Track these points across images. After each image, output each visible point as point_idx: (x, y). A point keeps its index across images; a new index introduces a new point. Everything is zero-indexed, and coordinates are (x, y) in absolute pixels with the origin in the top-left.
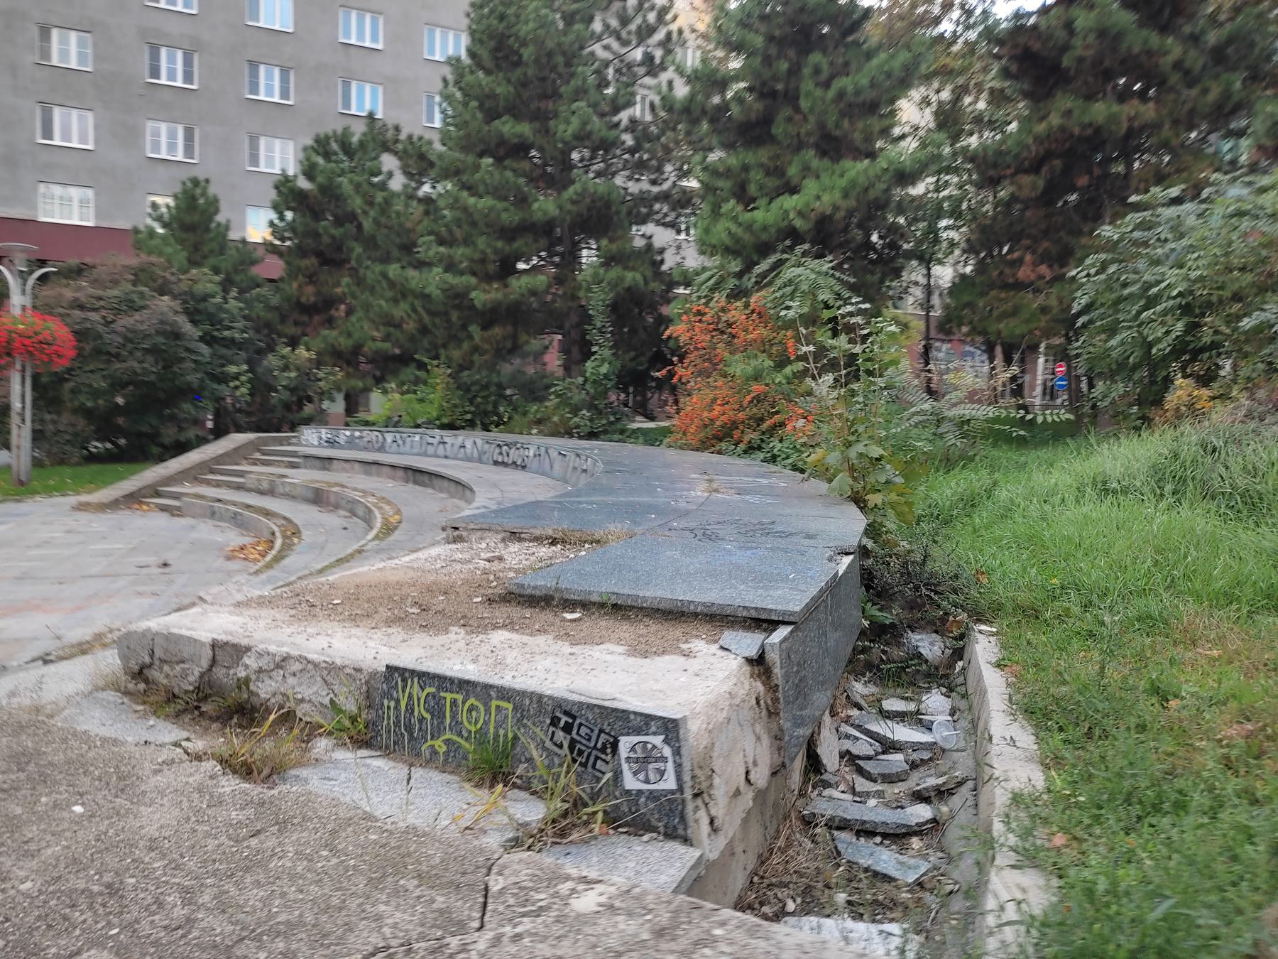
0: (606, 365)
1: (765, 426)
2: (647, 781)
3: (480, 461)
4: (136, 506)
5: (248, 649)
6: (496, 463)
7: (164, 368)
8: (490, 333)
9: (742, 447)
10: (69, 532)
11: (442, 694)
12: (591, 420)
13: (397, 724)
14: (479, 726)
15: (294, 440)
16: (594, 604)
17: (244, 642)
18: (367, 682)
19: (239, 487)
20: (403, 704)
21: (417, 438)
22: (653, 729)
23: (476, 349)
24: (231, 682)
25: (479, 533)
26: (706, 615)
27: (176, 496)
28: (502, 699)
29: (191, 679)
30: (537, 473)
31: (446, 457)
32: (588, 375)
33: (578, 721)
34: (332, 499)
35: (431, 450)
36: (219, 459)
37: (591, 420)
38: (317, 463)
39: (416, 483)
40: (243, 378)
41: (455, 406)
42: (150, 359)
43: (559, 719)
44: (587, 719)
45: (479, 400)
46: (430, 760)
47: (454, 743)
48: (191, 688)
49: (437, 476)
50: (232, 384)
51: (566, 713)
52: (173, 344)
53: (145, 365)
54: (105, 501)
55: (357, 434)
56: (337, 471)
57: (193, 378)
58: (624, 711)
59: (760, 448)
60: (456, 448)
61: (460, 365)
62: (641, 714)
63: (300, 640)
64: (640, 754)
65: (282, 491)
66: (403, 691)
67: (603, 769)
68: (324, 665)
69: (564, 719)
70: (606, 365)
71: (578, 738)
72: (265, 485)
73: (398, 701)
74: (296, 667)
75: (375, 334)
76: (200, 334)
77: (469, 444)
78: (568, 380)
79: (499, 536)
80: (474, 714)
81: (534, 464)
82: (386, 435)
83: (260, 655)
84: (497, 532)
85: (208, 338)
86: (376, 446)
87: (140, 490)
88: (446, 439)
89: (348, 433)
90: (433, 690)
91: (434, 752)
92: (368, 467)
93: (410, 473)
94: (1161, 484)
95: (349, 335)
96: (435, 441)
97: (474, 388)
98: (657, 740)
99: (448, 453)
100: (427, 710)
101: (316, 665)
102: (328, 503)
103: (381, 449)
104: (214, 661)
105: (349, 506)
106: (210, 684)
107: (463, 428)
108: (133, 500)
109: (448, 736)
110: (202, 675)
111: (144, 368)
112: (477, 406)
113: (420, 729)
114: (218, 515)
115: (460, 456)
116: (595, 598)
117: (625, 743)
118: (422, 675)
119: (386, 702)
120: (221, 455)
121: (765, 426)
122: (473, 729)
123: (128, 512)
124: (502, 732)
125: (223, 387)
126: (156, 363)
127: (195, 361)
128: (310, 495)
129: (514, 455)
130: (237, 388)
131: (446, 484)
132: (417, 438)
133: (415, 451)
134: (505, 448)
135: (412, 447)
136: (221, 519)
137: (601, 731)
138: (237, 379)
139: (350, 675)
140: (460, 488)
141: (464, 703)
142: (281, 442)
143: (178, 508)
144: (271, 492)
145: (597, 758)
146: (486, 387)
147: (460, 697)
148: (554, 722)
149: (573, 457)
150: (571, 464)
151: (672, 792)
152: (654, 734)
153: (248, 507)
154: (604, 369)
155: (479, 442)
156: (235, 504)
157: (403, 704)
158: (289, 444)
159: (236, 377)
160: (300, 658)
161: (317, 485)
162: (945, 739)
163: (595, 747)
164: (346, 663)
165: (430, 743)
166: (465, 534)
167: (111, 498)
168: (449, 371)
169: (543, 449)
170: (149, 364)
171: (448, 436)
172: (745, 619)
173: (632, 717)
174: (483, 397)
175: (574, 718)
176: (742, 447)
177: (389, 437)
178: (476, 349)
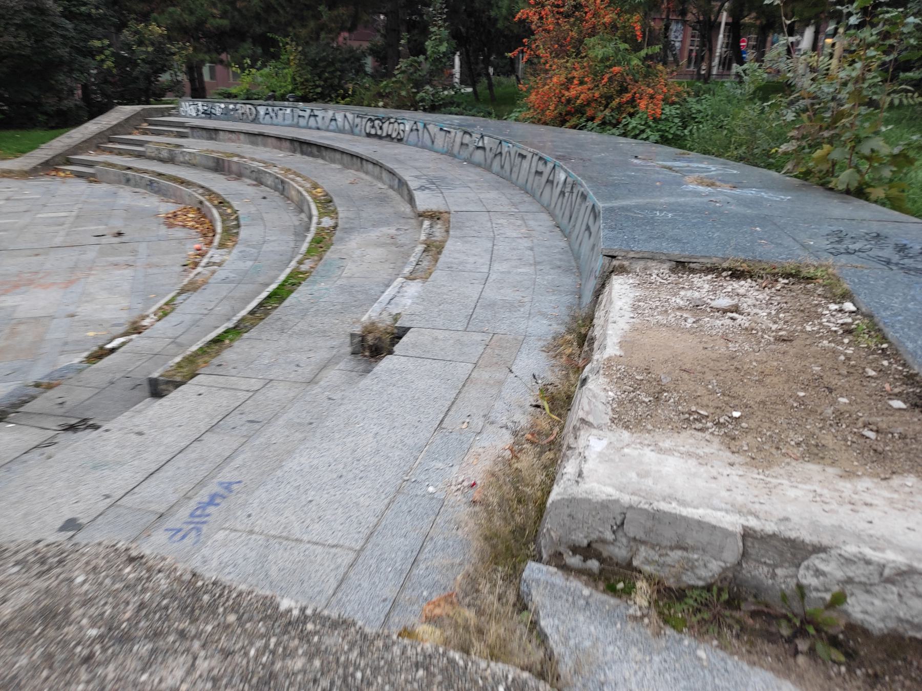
0: (445, 44)
1: (614, 104)
3: (352, 132)
4: (54, 173)
5: (819, 549)
6: (369, 135)
7: (36, 41)
8: (335, 13)
10: (8, 199)
15: (173, 112)
19: (140, 155)
21: (288, 111)
23: (322, 27)
25: (641, 264)
27: (90, 164)
29: (703, 573)
30: (416, 145)
31: (318, 129)
32: (428, 53)
34: (234, 168)
35: (302, 122)
36: (115, 129)
38: (204, 133)
39: (303, 153)
40: (107, 52)
41: (307, 80)
42: (23, 33)
49: (327, 148)
50: (98, 58)
52: (40, 19)
53: (19, 40)
54: (26, 168)
55: (231, 106)
56: (224, 141)
57: (64, 52)
60: (327, 120)
65: (182, 159)
70: (445, 44)
72: (165, 154)
75: (215, 11)
76: (61, 9)
77: (339, 117)
78: (412, 58)
79: (666, 266)
81: (413, 137)
82: (259, 108)
83: (848, 561)
84: (662, 262)
85: (67, 13)
86: (251, 118)
87: (54, 157)
88: (316, 113)
89: (223, 106)
92: (253, 138)
93: (297, 145)
95: (192, 12)
96: (307, 114)
97: (322, 64)
102: (230, 172)
103: (255, 120)
104: (745, 554)
105: (254, 175)
107: (315, 100)
108: (49, 167)
111: (19, 43)
112: (325, 80)
114: (132, 182)
115: (331, 128)
120: (116, 125)
121: (614, 104)
123: (47, 178)
125: (89, 60)
126: (29, 37)
127: (62, 36)
128: (211, 164)
130: (103, 61)
131: (338, 156)
132: (288, 111)
133: (287, 122)
134: (377, 122)
135: (284, 119)
136: (135, 186)
138: (102, 53)
142: (162, 112)
143: (93, 175)
144: (171, 160)
146: (332, 63)
149: (460, 134)
150: (458, 140)
153: (160, 175)
155: (350, 116)
156: (145, 172)
158: (170, 115)
159: (101, 51)
161: (215, 155)
166: (626, 263)
167: (31, 166)
169: (420, 126)
170: (22, 38)
174: (329, 73)
177: (262, 110)
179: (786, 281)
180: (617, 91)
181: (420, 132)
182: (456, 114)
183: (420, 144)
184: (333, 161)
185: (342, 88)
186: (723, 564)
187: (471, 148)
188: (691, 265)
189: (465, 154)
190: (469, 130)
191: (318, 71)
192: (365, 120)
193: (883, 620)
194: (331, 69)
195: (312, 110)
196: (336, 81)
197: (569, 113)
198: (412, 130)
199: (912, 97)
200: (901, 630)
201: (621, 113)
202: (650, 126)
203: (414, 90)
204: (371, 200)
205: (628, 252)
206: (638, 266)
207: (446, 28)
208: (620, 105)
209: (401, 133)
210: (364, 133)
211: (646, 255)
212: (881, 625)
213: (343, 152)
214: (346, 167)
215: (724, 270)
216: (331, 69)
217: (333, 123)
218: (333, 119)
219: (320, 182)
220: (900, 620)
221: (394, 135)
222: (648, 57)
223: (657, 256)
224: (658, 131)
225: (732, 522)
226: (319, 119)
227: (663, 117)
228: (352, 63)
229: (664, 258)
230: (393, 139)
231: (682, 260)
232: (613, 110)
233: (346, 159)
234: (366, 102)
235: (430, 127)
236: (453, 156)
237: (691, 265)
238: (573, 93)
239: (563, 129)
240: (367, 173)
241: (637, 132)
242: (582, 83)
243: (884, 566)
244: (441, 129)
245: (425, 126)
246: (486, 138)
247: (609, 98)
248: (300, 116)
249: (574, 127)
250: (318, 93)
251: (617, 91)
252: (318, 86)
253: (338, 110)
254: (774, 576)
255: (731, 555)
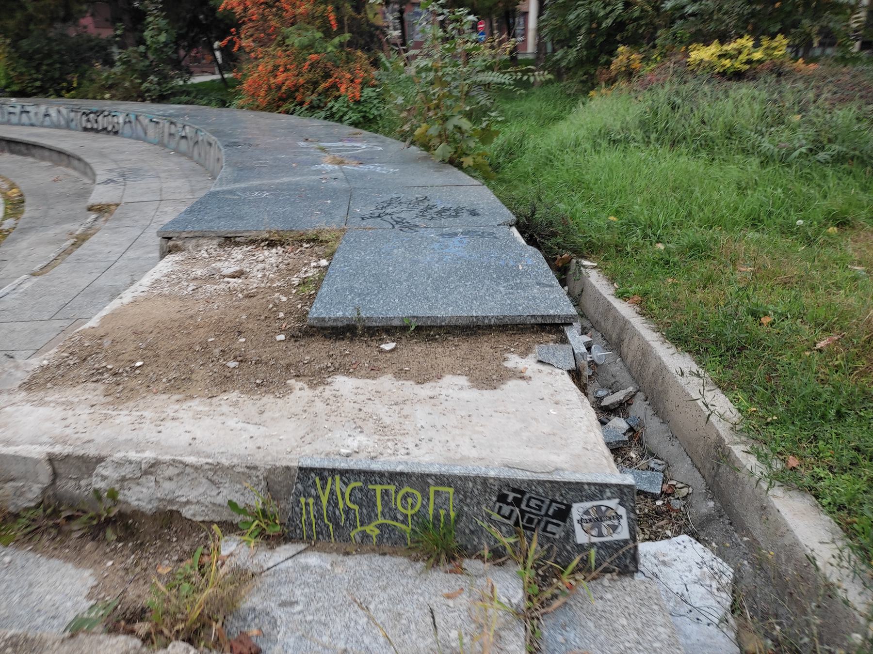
1: (320, 88)
2: (600, 535)
3: (68, 127)
5: (100, 460)
6: (85, 129)
9: (305, 106)
11: (370, 487)
12: (159, 84)
13: (319, 516)
14: (417, 509)
16: (396, 327)
17: (92, 451)
18: (265, 478)
20: (324, 500)
22: (609, 494)
23: (30, 19)
24: (88, 493)
25: (194, 242)
26: (499, 326)
28: (442, 484)
29: (31, 496)
30: (130, 137)
31: (32, 125)
32: (148, 43)
33: (527, 496)
35: (15, 119)
37: (159, 84)
39: (12, 152)
41: (22, 74)
43: (507, 496)
44: (538, 493)
45: (44, 67)
46: (364, 545)
47: (388, 526)
48: (33, 504)
49: (35, 146)
51: (514, 490)
58: (577, 483)
59: (319, 107)
60: (41, 116)
61: (17, 35)
62: (595, 484)
63: (148, 432)
64: (593, 515)
66: (323, 488)
67: (554, 531)
68: (207, 467)
69: (511, 496)
71: (528, 509)
73: (317, 498)
74: (171, 471)
77: (53, 112)
79: (216, 242)
80: (410, 500)
81: (127, 129)
83: (119, 464)
84: (212, 238)
88: (28, 109)
90: (359, 484)
91: (365, 536)
94: (647, 134)
96: (18, 110)
98: (613, 503)
99: (34, 121)
100: (354, 503)
101: (196, 468)
104: (55, 475)
106: (59, 499)
109: (381, 520)
110: (44, 491)
113: (347, 518)
115: (46, 123)
116: (396, 323)
117: (577, 510)
118: (344, 473)
119: (303, 500)
121: (320, 88)
122: (410, 512)
124: (442, 512)
129: (102, 122)
131: (47, 153)
137: (552, 501)
139: (244, 474)
140: (64, 158)
141: (396, 492)
145: (548, 523)
146: (49, 55)
147: (392, 488)
148: (502, 498)
149: (167, 124)
150: (166, 130)
151: (626, 542)
152: (609, 498)
154: (163, 38)
155: (64, 111)
157: (324, 500)
160: (173, 463)
162: (599, 358)
163: (547, 515)
164: (235, 461)
165: (359, 529)
166: (180, 243)
168: (8, 41)
169: (132, 117)
171: (28, 103)
172: (533, 325)
173: (586, 487)
174: (48, 65)
175: (523, 493)
176: (305, 106)
178: (30, 19)
179: (308, 245)
180: (322, 77)
181: (133, 124)
182: (186, 103)
183: (134, 135)
184: (43, 159)
185: (65, 80)
186: (40, 486)
187: (177, 138)
188: (237, 239)
189: (173, 144)
190: (174, 120)
191: (34, 64)
192: (79, 114)
193: (150, 502)
194: (49, 61)
195: (23, 106)
196: (57, 75)
197: (280, 99)
198: (125, 123)
199: (543, 75)
200: (161, 507)
201: (327, 96)
202: (351, 109)
203: (139, 81)
204: (68, 196)
205: (180, 233)
206: (190, 245)
207: (165, 17)
208: (327, 90)
209: (116, 125)
210: (80, 128)
211: (197, 234)
212: (150, 506)
213: (50, 150)
214: (57, 164)
215: (263, 241)
216: (49, 61)
217: (47, 118)
218: (47, 115)
219: (18, 182)
220: (161, 500)
221: (110, 128)
222: (341, 45)
223: (207, 234)
224: (360, 112)
225: (38, 452)
226: (32, 115)
227: (362, 99)
228: (97, 52)
229: (213, 235)
230: (109, 132)
231: (229, 235)
232: (320, 94)
233: (55, 156)
234: (90, 95)
235: (141, 118)
236: (164, 146)
237: (237, 239)
238: (281, 78)
239: (275, 115)
240: (75, 169)
241: (341, 114)
242: (286, 70)
243: (140, 462)
244: (151, 121)
245: (137, 117)
246: (187, 128)
247: (316, 84)
248: (10, 113)
249: (287, 112)
250: (37, 87)
251: (322, 77)
252: (36, 80)
253: (51, 104)
254: (80, 488)
255: (45, 478)
